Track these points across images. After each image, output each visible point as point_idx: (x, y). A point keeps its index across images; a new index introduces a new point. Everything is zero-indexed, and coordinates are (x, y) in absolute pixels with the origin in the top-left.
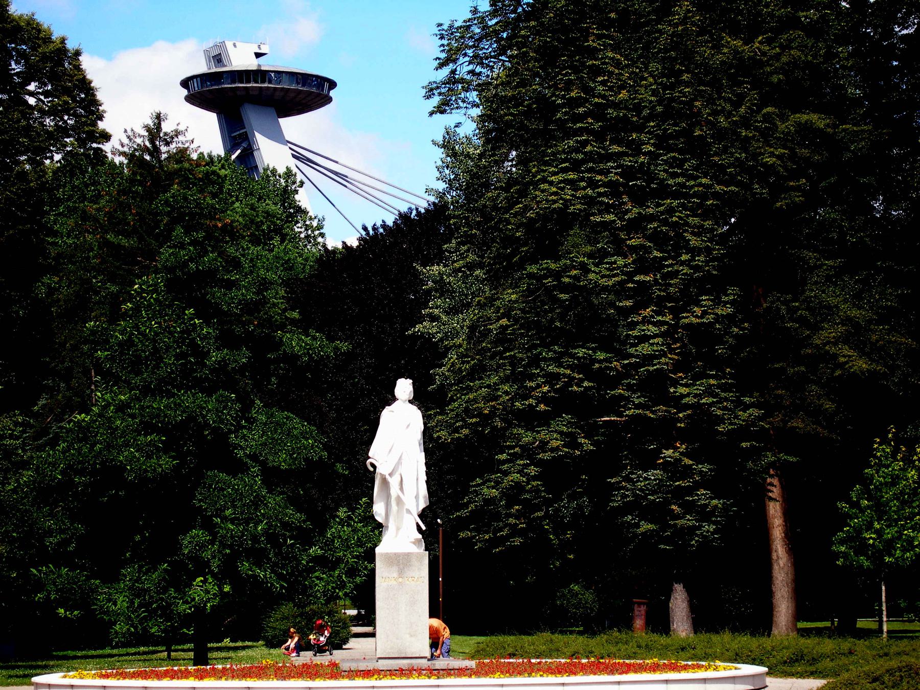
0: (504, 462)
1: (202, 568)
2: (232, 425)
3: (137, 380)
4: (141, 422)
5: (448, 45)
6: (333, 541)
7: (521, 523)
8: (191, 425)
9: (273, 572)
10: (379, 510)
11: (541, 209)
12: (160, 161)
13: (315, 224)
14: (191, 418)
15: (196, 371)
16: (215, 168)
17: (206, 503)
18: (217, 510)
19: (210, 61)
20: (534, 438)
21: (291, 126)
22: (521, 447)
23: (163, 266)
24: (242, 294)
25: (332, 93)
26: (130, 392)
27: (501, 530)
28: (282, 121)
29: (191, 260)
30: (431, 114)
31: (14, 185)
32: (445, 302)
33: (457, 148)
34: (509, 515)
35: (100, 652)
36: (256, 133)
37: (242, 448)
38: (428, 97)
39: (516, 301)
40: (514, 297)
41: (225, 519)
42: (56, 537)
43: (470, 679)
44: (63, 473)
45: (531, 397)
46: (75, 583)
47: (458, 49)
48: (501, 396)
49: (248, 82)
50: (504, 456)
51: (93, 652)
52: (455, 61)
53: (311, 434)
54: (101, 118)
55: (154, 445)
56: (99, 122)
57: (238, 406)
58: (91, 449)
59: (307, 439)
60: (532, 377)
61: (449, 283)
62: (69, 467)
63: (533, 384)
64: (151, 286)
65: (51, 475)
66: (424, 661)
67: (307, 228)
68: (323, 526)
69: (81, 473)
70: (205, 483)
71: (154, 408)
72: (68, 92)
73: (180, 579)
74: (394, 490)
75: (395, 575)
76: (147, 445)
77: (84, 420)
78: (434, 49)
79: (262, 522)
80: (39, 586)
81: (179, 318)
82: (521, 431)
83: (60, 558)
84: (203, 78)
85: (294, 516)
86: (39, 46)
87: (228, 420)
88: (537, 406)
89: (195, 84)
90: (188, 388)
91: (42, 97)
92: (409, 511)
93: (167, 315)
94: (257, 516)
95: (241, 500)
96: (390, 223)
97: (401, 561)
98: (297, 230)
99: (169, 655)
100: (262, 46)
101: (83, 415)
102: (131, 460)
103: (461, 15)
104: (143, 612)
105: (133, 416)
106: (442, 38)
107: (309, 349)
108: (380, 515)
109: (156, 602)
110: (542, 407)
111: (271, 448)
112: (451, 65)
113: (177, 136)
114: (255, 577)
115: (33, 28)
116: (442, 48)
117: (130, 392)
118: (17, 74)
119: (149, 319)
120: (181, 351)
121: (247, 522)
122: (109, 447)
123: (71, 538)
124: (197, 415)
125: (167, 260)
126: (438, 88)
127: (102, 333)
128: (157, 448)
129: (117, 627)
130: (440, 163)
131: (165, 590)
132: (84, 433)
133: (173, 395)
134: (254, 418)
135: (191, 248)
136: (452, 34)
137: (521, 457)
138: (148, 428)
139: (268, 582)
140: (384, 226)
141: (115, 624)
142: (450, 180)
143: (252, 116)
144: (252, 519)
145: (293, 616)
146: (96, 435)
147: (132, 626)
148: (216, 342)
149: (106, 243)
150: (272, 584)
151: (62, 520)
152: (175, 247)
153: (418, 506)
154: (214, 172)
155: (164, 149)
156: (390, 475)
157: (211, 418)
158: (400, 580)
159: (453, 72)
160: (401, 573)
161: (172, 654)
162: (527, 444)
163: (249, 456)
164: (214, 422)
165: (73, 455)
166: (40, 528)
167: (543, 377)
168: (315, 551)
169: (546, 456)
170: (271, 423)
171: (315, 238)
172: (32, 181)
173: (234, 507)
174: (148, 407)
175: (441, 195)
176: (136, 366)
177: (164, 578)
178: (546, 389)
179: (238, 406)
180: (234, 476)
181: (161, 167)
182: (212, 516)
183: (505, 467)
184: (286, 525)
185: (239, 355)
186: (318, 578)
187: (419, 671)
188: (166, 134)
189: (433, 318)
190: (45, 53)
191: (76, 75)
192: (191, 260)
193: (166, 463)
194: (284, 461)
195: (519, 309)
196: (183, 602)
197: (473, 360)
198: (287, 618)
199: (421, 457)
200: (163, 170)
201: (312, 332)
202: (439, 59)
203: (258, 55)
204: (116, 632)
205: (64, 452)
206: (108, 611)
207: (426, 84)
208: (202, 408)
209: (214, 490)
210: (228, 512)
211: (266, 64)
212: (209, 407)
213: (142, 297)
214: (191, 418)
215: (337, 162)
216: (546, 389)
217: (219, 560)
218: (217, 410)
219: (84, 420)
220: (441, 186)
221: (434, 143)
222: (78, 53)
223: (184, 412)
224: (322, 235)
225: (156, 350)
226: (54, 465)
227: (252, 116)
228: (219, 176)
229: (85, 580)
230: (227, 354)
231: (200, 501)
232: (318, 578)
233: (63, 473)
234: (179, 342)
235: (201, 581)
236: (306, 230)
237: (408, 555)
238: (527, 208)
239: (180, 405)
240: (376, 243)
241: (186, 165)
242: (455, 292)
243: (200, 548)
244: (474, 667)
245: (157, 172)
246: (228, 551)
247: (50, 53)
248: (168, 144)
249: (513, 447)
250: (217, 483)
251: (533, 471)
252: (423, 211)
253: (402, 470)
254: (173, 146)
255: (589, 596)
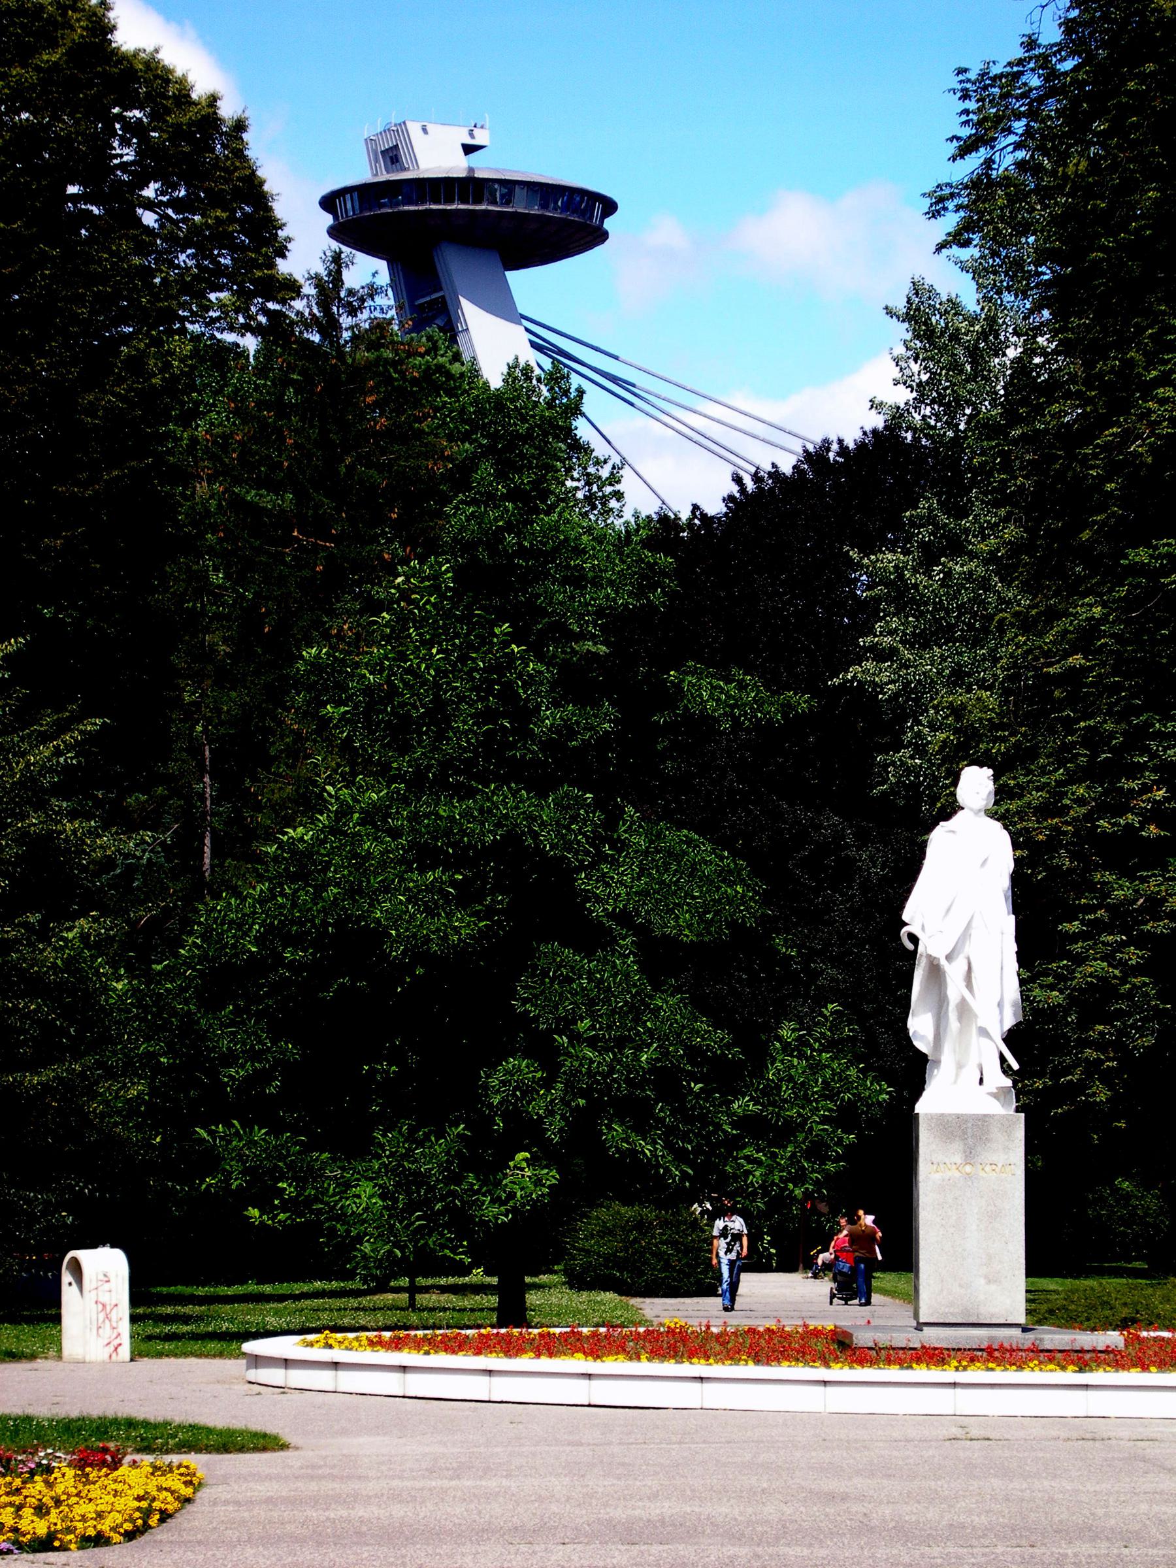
0: (1075, 938)
1: (524, 1132)
2: (587, 853)
3: (403, 764)
4: (413, 845)
5: (980, 110)
6: (779, 1088)
7: (1109, 1059)
8: (513, 849)
9: (668, 1146)
10: (920, 1027)
11: (1159, 437)
12: (339, 348)
13: (605, 473)
14: (512, 839)
15: (513, 746)
16: (441, 360)
17: (536, 1006)
18: (558, 1020)
19: (377, 161)
20: (1136, 891)
21: (525, 284)
22: (1110, 908)
23: (454, 539)
24: (607, 596)
25: (608, 224)
26: (389, 787)
27: (1068, 1071)
28: (512, 276)
29: (509, 528)
30: (941, 247)
31: (120, 381)
32: (906, 624)
33: (934, 320)
34: (1084, 1043)
35: (237, 1289)
36: (461, 298)
37: (598, 899)
38: (934, 214)
39: (1104, 619)
40: (1097, 611)
41: (575, 1038)
42: (243, 1066)
43: (1146, 1375)
44: (259, 941)
45: (1131, 810)
46: (282, 1158)
47: (998, 119)
48: (1069, 808)
49: (478, 201)
50: (1074, 927)
51: (224, 1290)
52: (990, 142)
53: (739, 874)
54: (282, 252)
55: (441, 891)
56: (279, 261)
57: (598, 817)
58: (317, 897)
59: (731, 884)
60: (1135, 771)
61: (915, 586)
62: (270, 929)
63: (1134, 785)
64: (428, 578)
65: (234, 946)
66: (1017, 1332)
67: (589, 480)
68: (759, 1057)
69: (295, 941)
70: (535, 967)
71: (440, 817)
72: (215, 199)
73: (485, 1157)
74: (955, 988)
75: (958, 1159)
76: (427, 890)
77: (301, 839)
78: (950, 117)
79: (649, 1046)
80: (210, 1161)
81: (483, 644)
82: (1110, 877)
83: (251, 1107)
84: (366, 193)
85: (713, 1037)
86: (168, 112)
87: (578, 842)
88: (1142, 828)
89: (349, 206)
90: (504, 780)
91: (170, 212)
92: (983, 1032)
93: (457, 635)
94: (638, 1034)
95: (607, 1001)
96: (786, 468)
97: (968, 1131)
98: (569, 483)
99: (412, 1299)
100: (476, 132)
101: (300, 830)
102: (395, 918)
103: (1004, 52)
104: (419, 1218)
105: (395, 833)
106: (965, 96)
107: (732, 707)
108: (923, 1038)
109: (443, 1198)
110: (1153, 830)
111: (658, 901)
112: (982, 150)
113: (372, 296)
114: (633, 1153)
115: (157, 77)
116: (964, 118)
117: (389, 787)
118: (124, 166)
119: (424, 643)
120: (487, 707)
121: (621, 1043)
122: (353, 892)
123: (273, 1068)
124: (523, 833)
125: (463, 529)
126: (952, 196)
127: (334, 670)
128: (445, 895)
129: (367, 1248)
130: (900, 350)
131: (457, 1179)
132: (303, 866)
133: (471, 793)
134: (623, 842)
135: (510, 505)
136: (985, 88)
137: (1110, 929)
138: (425, 856)
139: (659, 1166)
140: (776, 474)
141: (359, 1239)
142: (920, 384)
143: (456, 266)
144: (630, 1039)
145: (623, 1228)
146: (326, 869)
147: (396, 1245)
148: (552, 689)
149: (237, 503)
150: (667, 1170)
151: (255, 1033)
152: (474, 502)
153: (1001, 1021)
154: (440, 368)
155: (346, 321)
156: (949, 958)
157: (547, 839)
158: (968, 1169)
159: (988, 163)
160: (970, 1155)
161: (418, 1297)
162: (1122, 904)
163: (611, 916)
164: (552, 848)
165: (282, 906)
166: (213, 1049)
167: (1154, 770)
168: (742, 1105)
169: (1161, 927)
170: (658, 852)
171: (605, 500)
172: (155, 375)
173: (592, 1015)
174: (427, 816)
175: (897, 417)
176: (400, 734)
177: (459, 1152)
178: (1160, 794)
179: (598, 817)
180: (590, 955)
181: (341, 355)
182: (550, 1031)
183: (1077, 947)
184: (694, 1053)
185: (596, 716)
186: (748, 1158)
187: (995, 1355)
188: (351, 292)
189: (883, 655)
190: (180, 125)
191: (236, 169)
192: (509, 528)
193: (464, 925)
194: (690, 926)
195: (1112, 636)
196: (493, 1201)
197: (1012, 734)
198: (611, 1232)
199: (1009, 923)
200: (344, 362)
201: (737, 673)
202: (958, 138)
203: (469, 149)
204: (365, 1257)
205: (262, 901)
206: (344, 1214)
207: (929, 187)
208: (531, 818)
209: (552, 980)
210: (583, 1025)
211: (486, 166)
212: (544, 818)
213: (410, 602)
214: (512, 839)
215: (616, 358)
216: (1160, 794)
217: (563, 1117)
218: (557, 823)
219: (301, 839)
220: (903, 396)
221: (889, 312)
222: (240, 126)
223: (499, 825)
224: (619, 496)
225: (439, 704)
226: (240, 926)
227: (456, 266)
228: (449, 375)
229: (299, 1153)
230: (574, 714)
231: (525, 1001)
232: (748, 1158)
233: (259, 941)
234: (483, 688)
235: (526, 1160)
236: (589, 483)
237: (984, 1119)
238: (1128, 436)
239: (490, 811)
240: (766, 505)
241: (388, 354)
242: (926, 604)
243: (524, 1094)
244: (1121, 1346)
245: (333, 366)
246: (582, 1102)
247: (189, 125)
248: (353, 312)
249: (1093, 909)
250: (559, 966)
251: (1133, 956)
252: (852, 446)
253: (969, 949)
254: (365, 315)
255: (1151, 1201)
